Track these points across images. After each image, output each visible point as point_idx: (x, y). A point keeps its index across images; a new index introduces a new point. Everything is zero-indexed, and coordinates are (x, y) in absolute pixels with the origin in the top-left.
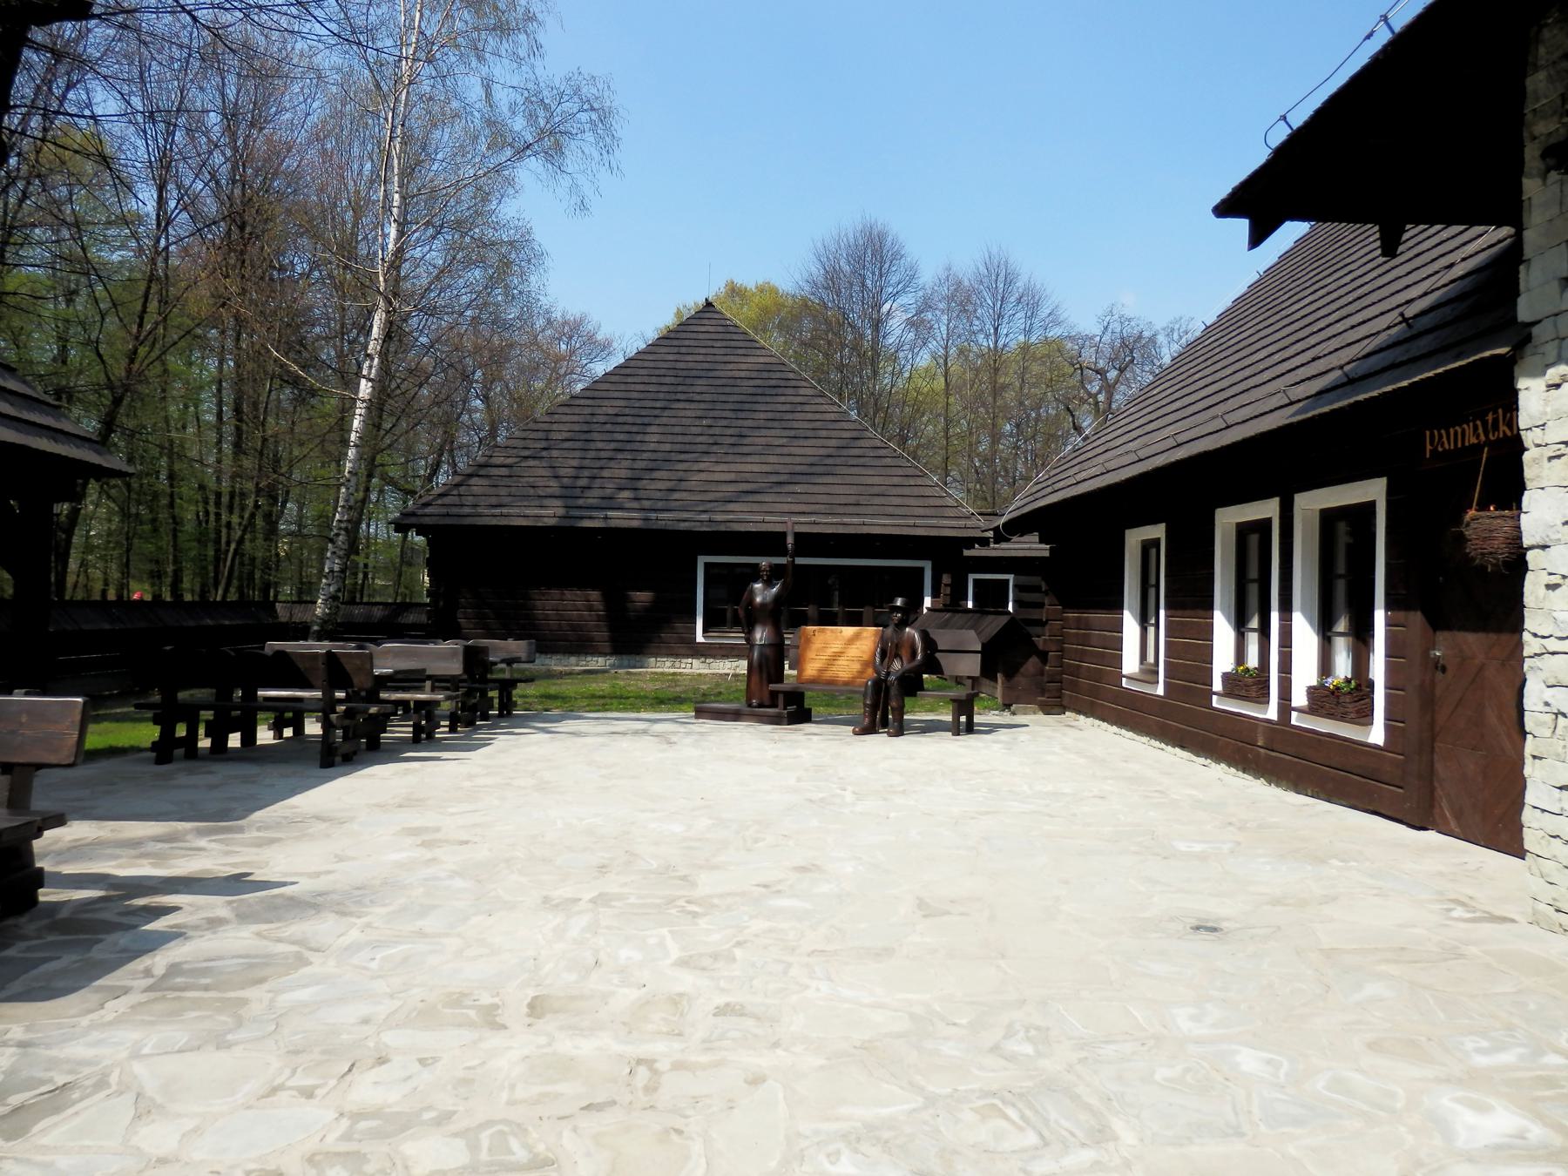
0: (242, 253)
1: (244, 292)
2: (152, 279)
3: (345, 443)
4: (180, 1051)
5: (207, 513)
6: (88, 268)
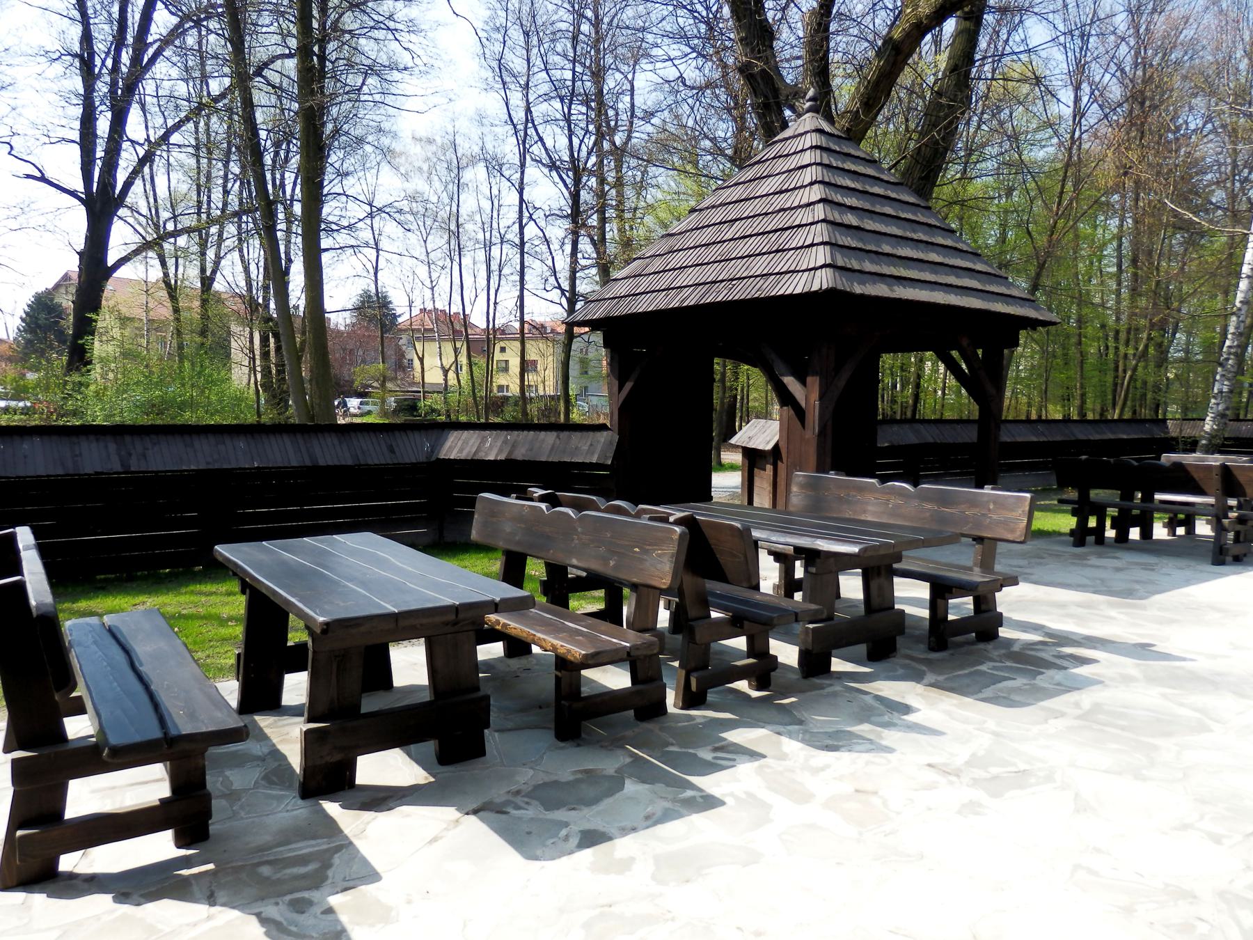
0: (1143, 124)
1: (1142, 158)
2: (1067, 166)
3: (1238, 275)
4: (1105, 772)
5: (1107, 348)
6: (1021, 167)
